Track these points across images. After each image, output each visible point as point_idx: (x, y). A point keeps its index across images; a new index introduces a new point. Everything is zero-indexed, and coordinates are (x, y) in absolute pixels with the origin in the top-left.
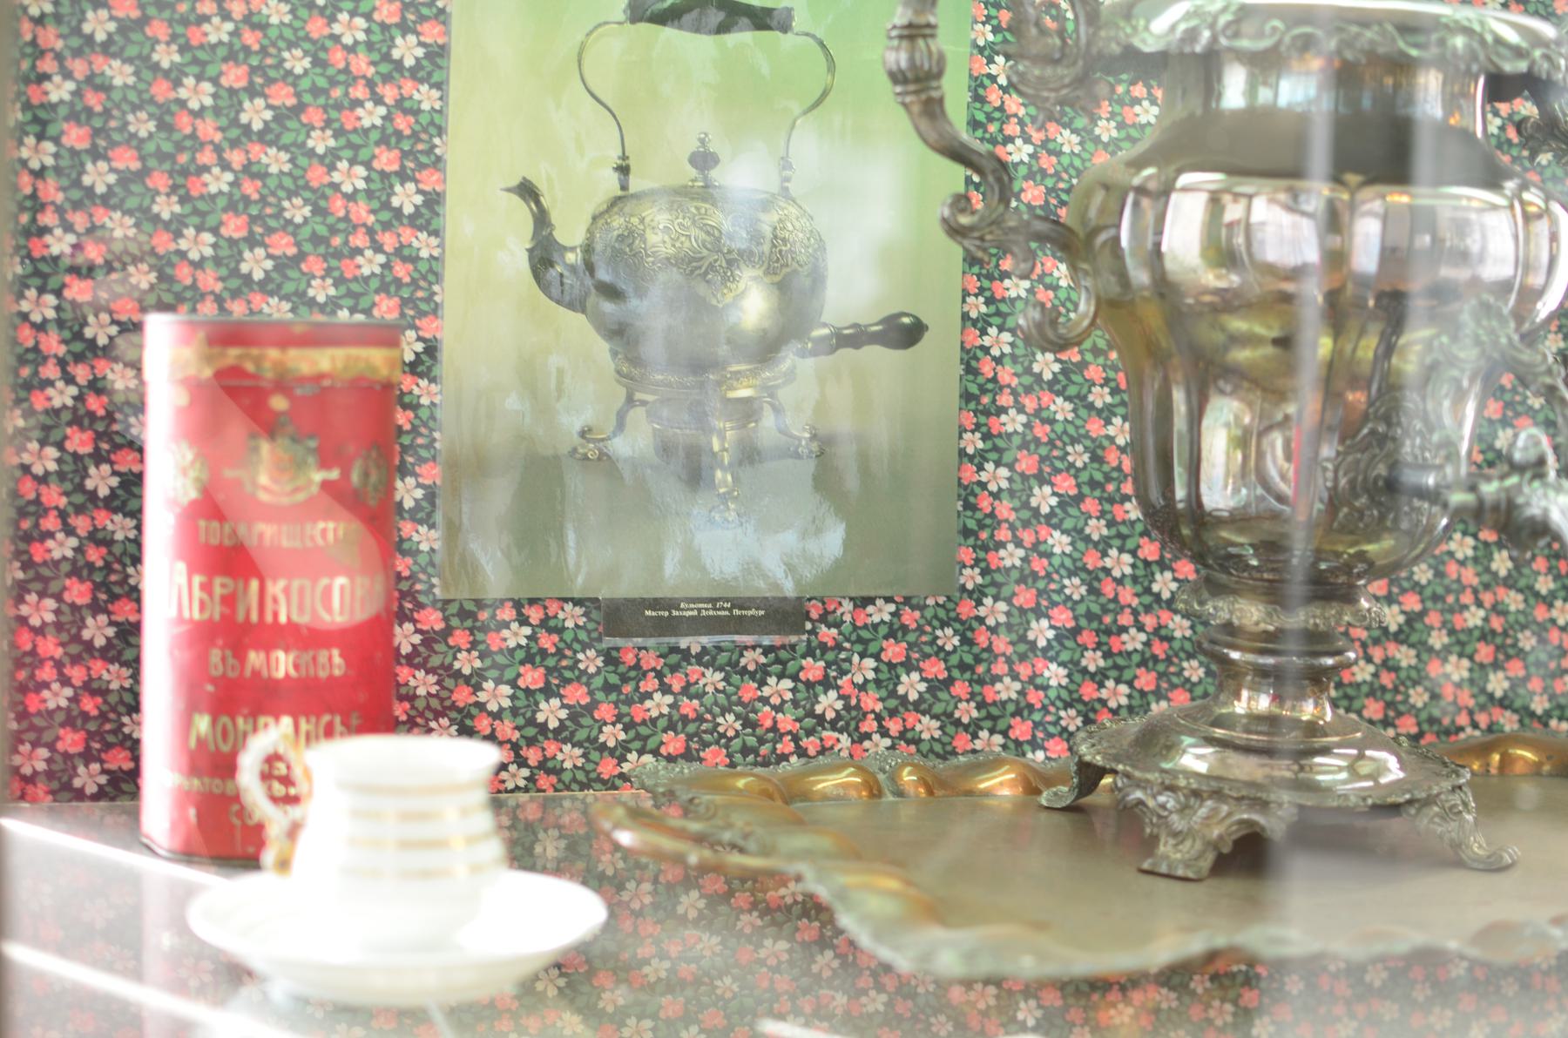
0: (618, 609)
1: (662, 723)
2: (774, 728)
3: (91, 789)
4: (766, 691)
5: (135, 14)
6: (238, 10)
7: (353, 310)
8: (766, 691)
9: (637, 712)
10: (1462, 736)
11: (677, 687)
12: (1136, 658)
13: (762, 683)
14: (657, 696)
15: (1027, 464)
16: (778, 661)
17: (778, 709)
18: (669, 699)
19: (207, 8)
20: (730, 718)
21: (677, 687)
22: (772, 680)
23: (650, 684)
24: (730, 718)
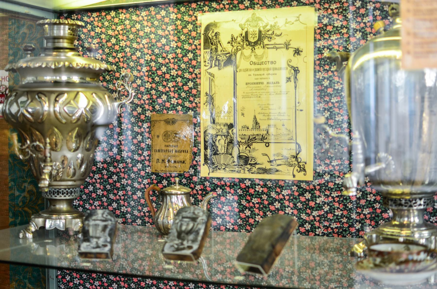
0: (92, 109)
1: (365, 207)
2: (339, 204)
3: (247, 180)
4: (341, 212)
5: (185, 287)
6: (168, 287)
7: (200, 5)
8: (341, 212)
9: (371, 210)
10: (227, 2)
11: (362, 215)
12: (170, 81)
13: (342, 214)
14: (366, 213)
15: (329, 28)
16: (338, 219)
17: (338, 208)
18: (364, 212)
19: (173, 288)
20: (350, 207)
21: (362, 215)
22: (340, 215)
23: (368, 216)
24: (350, 207)
